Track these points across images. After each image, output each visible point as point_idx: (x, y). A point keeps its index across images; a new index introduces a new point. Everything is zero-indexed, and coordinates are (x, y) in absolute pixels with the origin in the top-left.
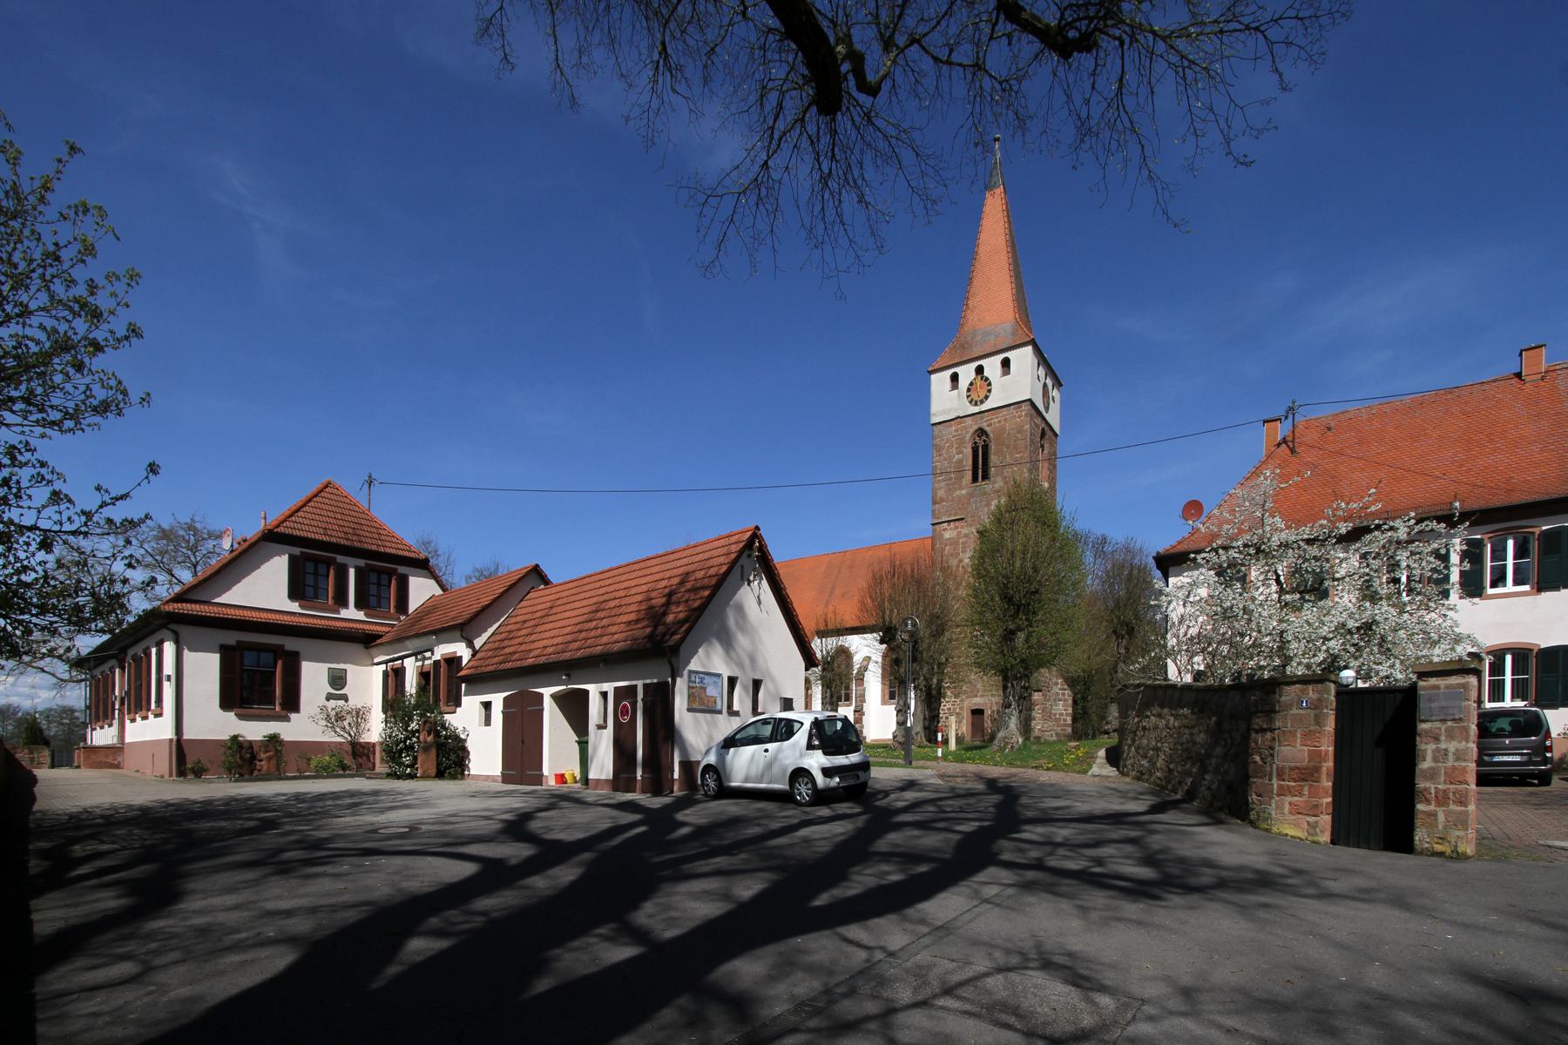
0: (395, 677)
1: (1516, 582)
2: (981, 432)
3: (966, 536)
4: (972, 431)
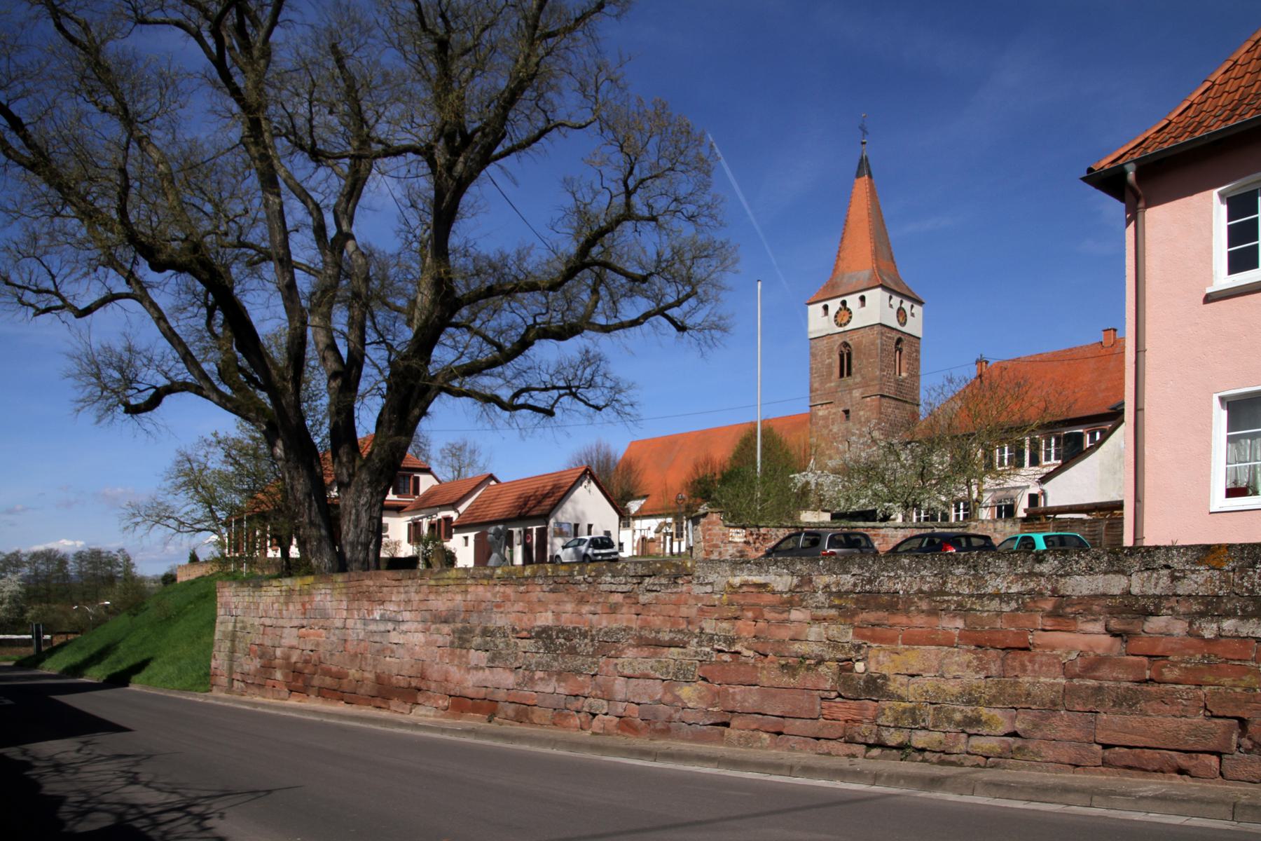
0: (415, 527)
1: (1056, 459)
2: (846, 344)
3: (834, 414)
4: (839, 343)
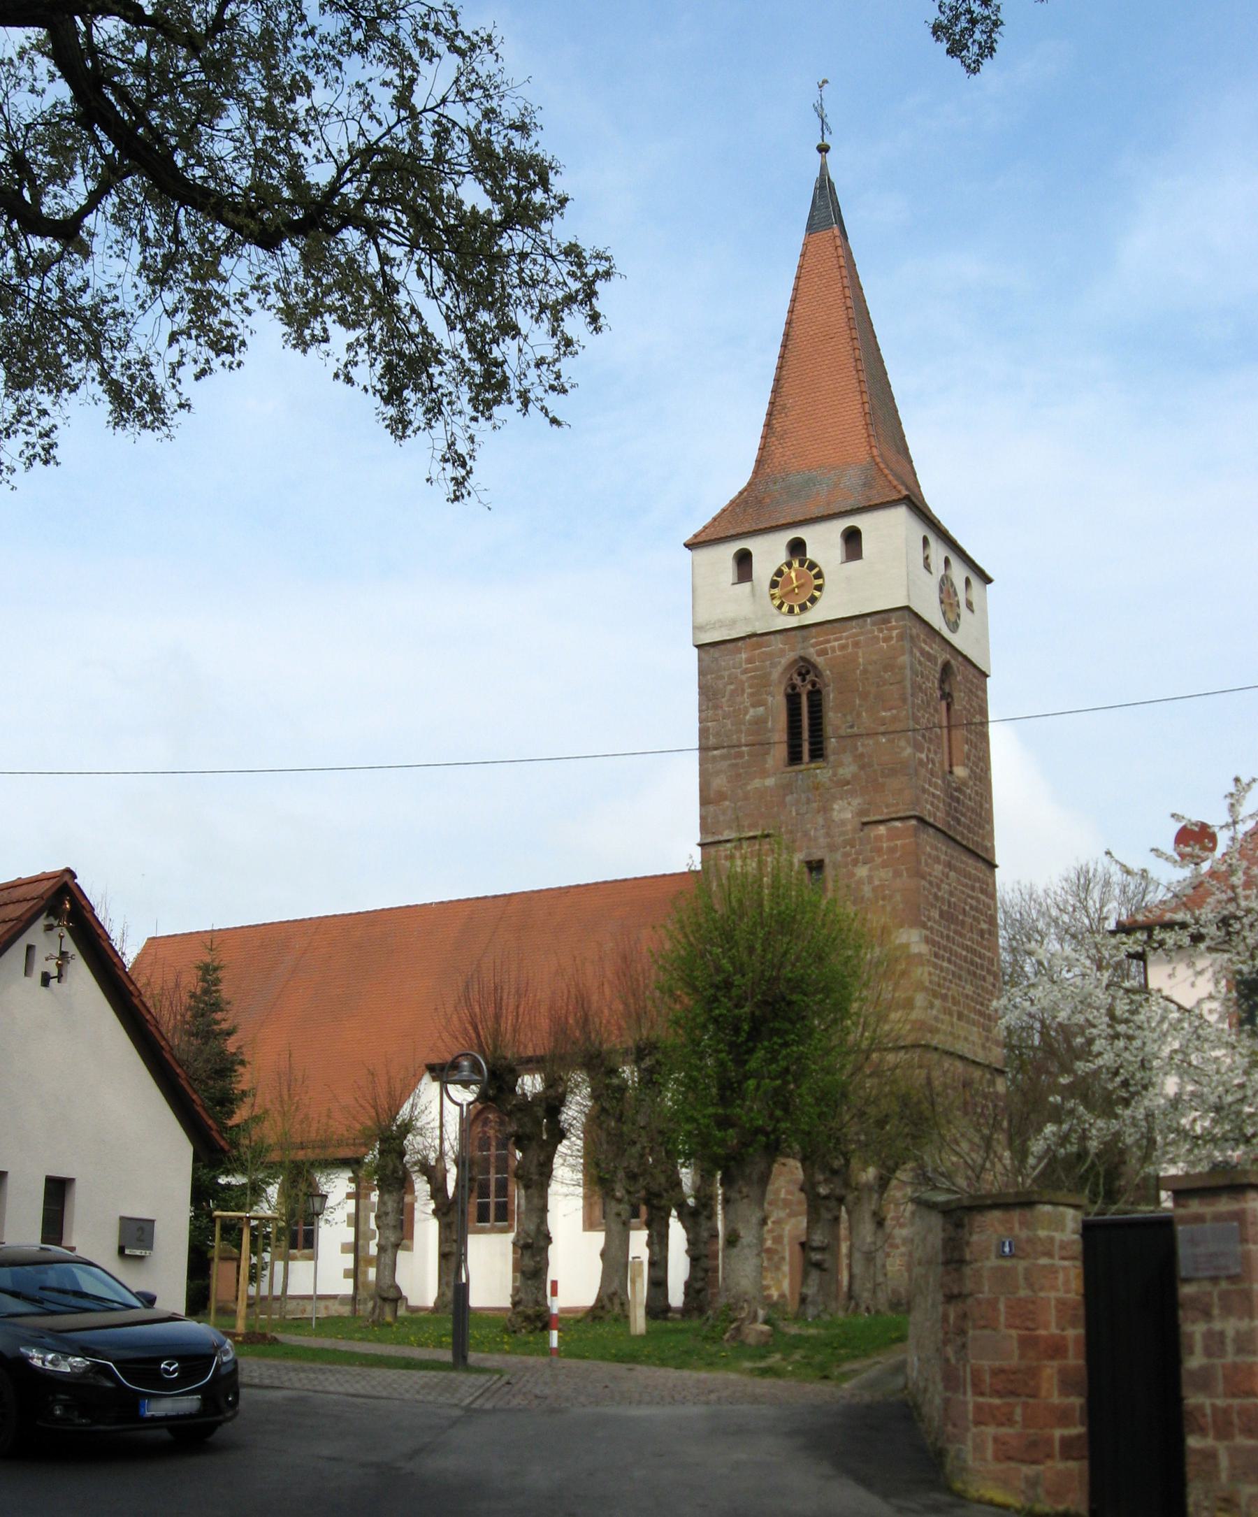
2: (805, 668)
4: (784, 661)
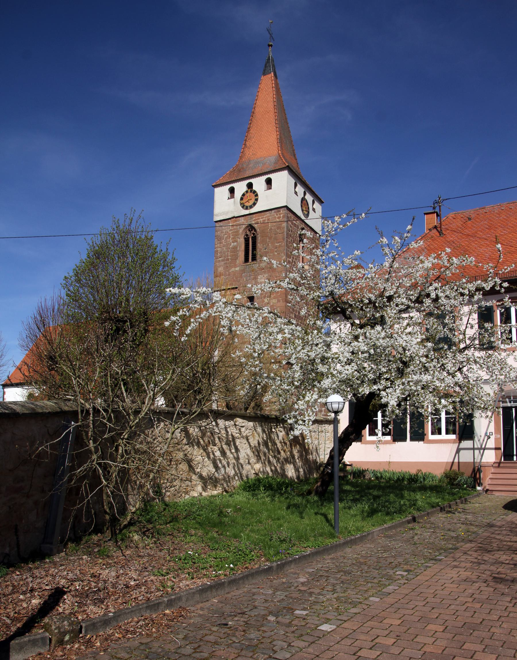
2: (251, 228)
